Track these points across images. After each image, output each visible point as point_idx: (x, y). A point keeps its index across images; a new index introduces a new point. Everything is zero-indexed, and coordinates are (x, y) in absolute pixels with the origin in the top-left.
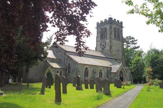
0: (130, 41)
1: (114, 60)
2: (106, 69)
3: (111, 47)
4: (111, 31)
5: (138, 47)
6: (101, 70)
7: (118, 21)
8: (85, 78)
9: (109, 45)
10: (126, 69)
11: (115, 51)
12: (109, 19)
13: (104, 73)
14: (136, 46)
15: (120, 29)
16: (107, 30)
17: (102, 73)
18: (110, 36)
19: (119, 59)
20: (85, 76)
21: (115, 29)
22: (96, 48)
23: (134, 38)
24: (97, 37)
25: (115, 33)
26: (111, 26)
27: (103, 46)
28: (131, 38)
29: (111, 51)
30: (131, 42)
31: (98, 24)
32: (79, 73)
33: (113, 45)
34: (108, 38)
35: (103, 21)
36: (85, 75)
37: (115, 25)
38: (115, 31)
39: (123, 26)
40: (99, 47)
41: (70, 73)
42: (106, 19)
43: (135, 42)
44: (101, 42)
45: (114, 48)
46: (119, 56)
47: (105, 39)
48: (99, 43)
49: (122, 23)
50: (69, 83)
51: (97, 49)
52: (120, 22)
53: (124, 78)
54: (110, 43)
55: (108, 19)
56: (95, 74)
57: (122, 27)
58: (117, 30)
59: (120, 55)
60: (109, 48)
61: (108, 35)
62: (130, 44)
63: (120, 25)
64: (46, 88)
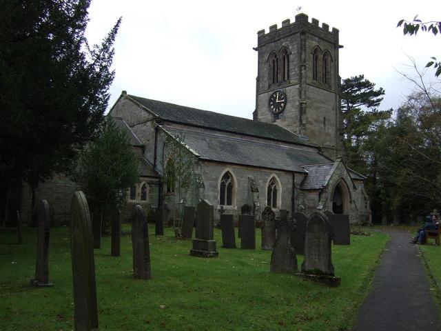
11: (316, 121)
15: (332, 51)
44: (271, 93)
49: (336, 31)
52: (331, 30)
58: (321, 56)
59: (329, 135)
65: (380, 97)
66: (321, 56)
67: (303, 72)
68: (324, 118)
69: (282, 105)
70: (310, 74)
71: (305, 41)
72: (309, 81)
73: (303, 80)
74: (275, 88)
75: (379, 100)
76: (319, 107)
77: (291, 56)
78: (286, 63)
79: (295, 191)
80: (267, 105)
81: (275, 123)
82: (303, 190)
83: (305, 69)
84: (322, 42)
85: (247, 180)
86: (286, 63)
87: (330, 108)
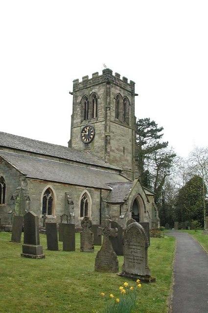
0: (146, 131)
1: (114, 172)
2: (99, 193)
3: (107, 141)
4: (108, 100)
5: (165, 145)
6: (85, 195)
7: (125, 79)
8: (44, 218)
9: (103, 136)
10: (147, 195)
11: (118, 150)
12: (104, 71)
13: (93, 204)
14: (161, 141)
15: (130, 98)
16: (99, 100)
17: (87, 204)
18: (106, 114)
19: (126, 171)
20: (44, 212)
21: (118, 96)
22: (70, 143)
23: (156, 123)
24: (73, 117)
25: (117, 107)
26: (109, 88)
27: (87, 137)
28: (149, 125)
29: (108, 150)
30: (148, 132)
31: (76, 83)
32: (29, 204)
33: (111, 134)
34: (101, 118)
35: (90, 77)
36: (44, 208)
37: (118, 88)
38: (118, 103)
39: (136, 93)
40: (78, 139)
41: (4, 203)
42: (97, 73)
43: (159, 134)
44: (82, 127)
45: (114, 144)
46: (125, 163)
47: (93, 121)
48: (78, 130)
49: (133, 84)
51: (73, 145)
53: (141, 216)
54: (106, 131)
55: (101, 73)
56: (71, 206)
57: (133, 94)
59: (127, 161)
60: (103, 144)
61: (101, 112)
62: (148, 136)
63: (129, 88)
64: (79, 82)
69: (92, 136)
74: (85, 123)
78: (95, 105)
83: (110, 110)
84: (122, 91)
85: (63, 195)
86: (95, 105)
87: (128, 140)
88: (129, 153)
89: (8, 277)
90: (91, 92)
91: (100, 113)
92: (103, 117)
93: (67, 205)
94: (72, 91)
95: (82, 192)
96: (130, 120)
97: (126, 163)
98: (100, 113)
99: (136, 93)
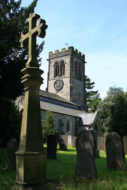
11: (76, 94)
15: (82, 64)
25: (76, 69)
37: (77, 58)
42: (52, 52)
44: (55, 80)
49: (84, 56)
50: (39, 66)
51: (49, 91)
52: (82, 55)
58: (78, 66)
59: (81, 101)
65: (93, 85)
66: (78, 66)
67: (72, 72)
68: (79, 93)
69: (61, 86)
70: (74, 73)
71: (73, 58)
72: (74, 76)
73: (72, 75)
74: (57, 78)
75: (93, 87)
76: (77, 88)
77: (66, 65)
78: (63, 67)
79: (77, 126)
80: (53, 85)
81: (57, 94)
82: (80, 125)
83: (72, 71)
84: (79, 60)
85: (58, 120)
86: (63, 67)
87: (81, 89)
88: (82, 96)
89: (124, 164)
90: (61, 60)
91: (67, 72)
92: (68, 75)
93: (61, 126)
94: (48, 59)
95: (67, 118)
96: (82, 77)
97: (80, 102)
98: (67, 72)
99: (85, 61)
